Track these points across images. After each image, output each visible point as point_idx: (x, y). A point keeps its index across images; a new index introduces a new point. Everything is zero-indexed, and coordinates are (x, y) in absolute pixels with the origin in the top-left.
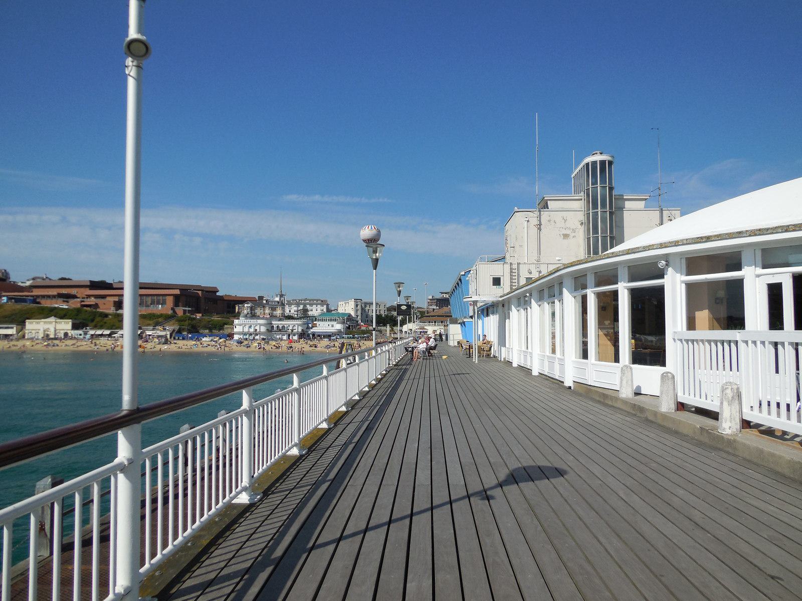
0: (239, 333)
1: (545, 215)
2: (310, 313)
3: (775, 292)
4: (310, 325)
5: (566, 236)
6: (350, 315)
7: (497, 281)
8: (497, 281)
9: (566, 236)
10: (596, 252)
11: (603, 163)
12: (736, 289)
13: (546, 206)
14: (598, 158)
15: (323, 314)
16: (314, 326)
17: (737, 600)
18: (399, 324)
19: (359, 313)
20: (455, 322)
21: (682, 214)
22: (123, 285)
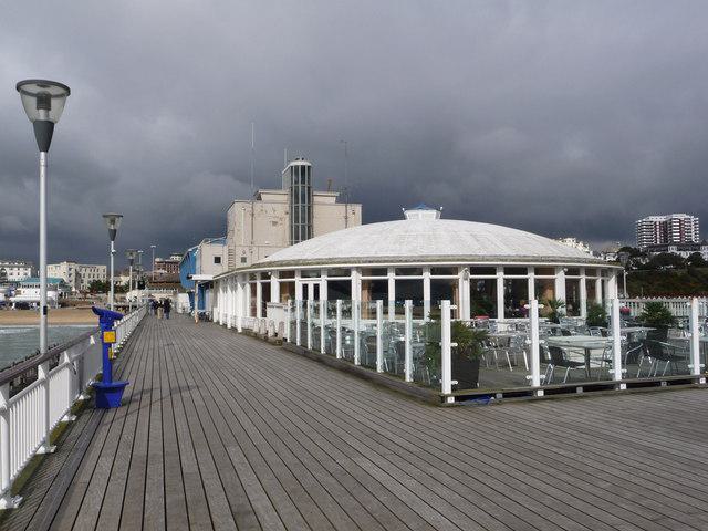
0: (259, 281)
1: (258, 205)
2: (10, 278)
3: (305, 287)
4: (13, 292)
5: (275, 223)
6: (62, 281)
7: (218, 260)
8: (218, 260)
9: (275, 223)
10: (297, 238)
11: (303, 167)
12: (292, 285)
13: (259, 198)
14: (300, 163)
15: (27, 280)
16: (18, 293)
17: (479, 528)
18: (510, 276)
19: (73, 277)
20: (183, 291)
21: (366, 220)
22: (334, 228)
